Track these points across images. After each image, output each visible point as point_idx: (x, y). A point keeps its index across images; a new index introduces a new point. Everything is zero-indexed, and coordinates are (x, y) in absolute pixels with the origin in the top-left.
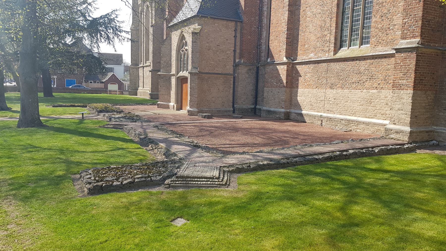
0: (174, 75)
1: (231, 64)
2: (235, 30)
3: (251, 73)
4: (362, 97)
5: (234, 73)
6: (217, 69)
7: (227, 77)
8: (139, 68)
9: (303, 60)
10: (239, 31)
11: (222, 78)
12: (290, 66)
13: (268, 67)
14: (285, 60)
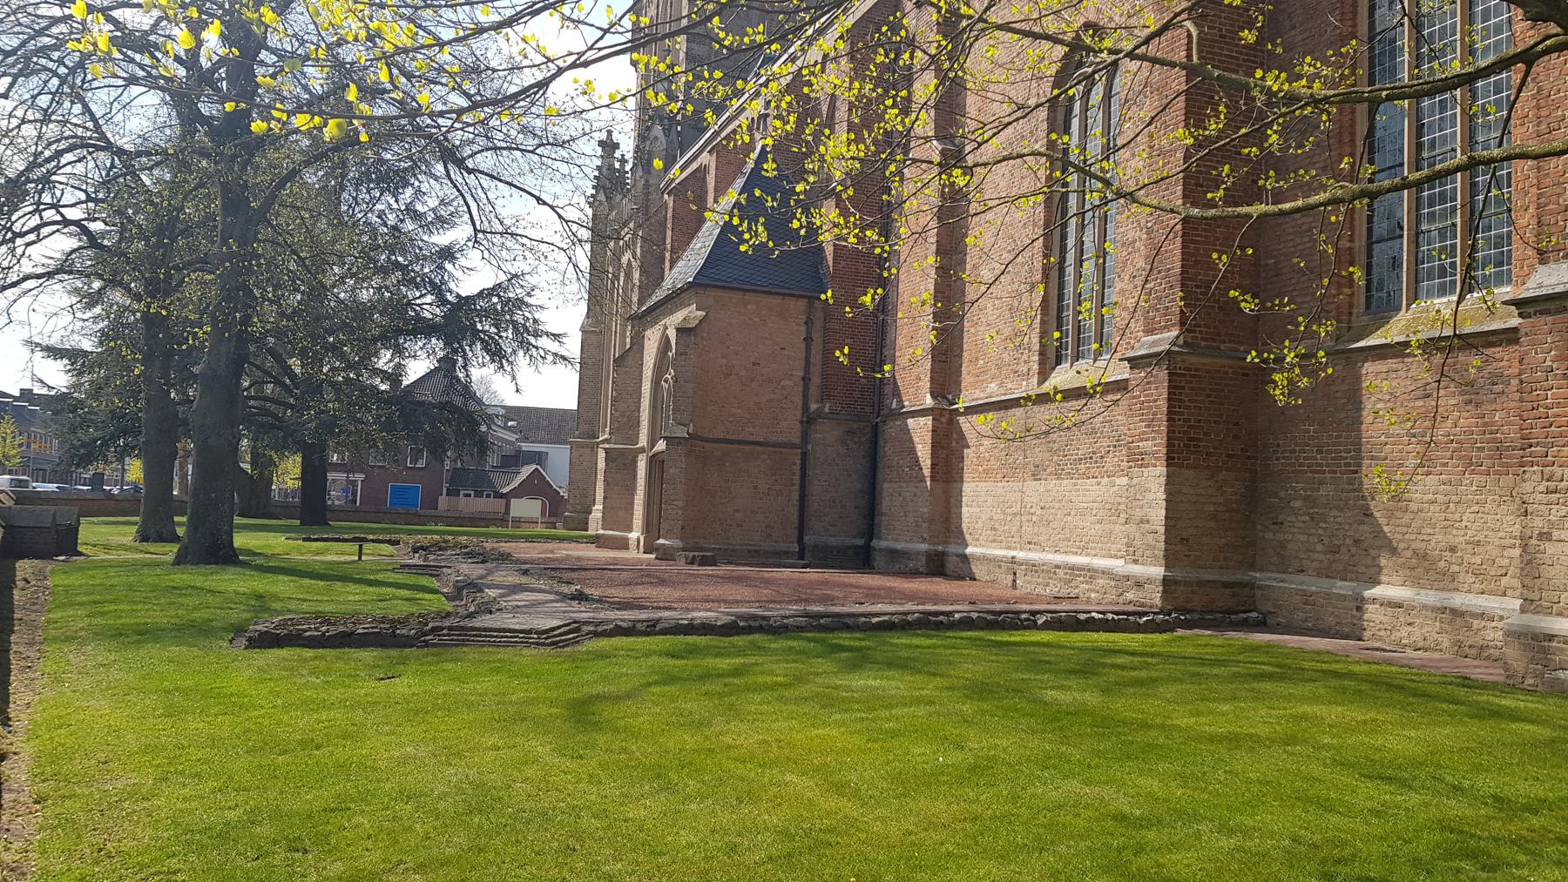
0: (642, 450)
1: (795, 415)
2: (809, 323)
3: (855, 443)
4: (1099, 499)
5: (802, 441)
6: (751, 429)
7: (781, 453)
8: (598, 444)
9: (973, 400)
10: (818, 324)
11: (765, 456)
12: (944, 420)
13: (891, 424)
14: (929, 401)
